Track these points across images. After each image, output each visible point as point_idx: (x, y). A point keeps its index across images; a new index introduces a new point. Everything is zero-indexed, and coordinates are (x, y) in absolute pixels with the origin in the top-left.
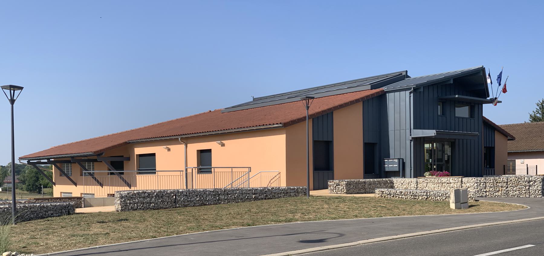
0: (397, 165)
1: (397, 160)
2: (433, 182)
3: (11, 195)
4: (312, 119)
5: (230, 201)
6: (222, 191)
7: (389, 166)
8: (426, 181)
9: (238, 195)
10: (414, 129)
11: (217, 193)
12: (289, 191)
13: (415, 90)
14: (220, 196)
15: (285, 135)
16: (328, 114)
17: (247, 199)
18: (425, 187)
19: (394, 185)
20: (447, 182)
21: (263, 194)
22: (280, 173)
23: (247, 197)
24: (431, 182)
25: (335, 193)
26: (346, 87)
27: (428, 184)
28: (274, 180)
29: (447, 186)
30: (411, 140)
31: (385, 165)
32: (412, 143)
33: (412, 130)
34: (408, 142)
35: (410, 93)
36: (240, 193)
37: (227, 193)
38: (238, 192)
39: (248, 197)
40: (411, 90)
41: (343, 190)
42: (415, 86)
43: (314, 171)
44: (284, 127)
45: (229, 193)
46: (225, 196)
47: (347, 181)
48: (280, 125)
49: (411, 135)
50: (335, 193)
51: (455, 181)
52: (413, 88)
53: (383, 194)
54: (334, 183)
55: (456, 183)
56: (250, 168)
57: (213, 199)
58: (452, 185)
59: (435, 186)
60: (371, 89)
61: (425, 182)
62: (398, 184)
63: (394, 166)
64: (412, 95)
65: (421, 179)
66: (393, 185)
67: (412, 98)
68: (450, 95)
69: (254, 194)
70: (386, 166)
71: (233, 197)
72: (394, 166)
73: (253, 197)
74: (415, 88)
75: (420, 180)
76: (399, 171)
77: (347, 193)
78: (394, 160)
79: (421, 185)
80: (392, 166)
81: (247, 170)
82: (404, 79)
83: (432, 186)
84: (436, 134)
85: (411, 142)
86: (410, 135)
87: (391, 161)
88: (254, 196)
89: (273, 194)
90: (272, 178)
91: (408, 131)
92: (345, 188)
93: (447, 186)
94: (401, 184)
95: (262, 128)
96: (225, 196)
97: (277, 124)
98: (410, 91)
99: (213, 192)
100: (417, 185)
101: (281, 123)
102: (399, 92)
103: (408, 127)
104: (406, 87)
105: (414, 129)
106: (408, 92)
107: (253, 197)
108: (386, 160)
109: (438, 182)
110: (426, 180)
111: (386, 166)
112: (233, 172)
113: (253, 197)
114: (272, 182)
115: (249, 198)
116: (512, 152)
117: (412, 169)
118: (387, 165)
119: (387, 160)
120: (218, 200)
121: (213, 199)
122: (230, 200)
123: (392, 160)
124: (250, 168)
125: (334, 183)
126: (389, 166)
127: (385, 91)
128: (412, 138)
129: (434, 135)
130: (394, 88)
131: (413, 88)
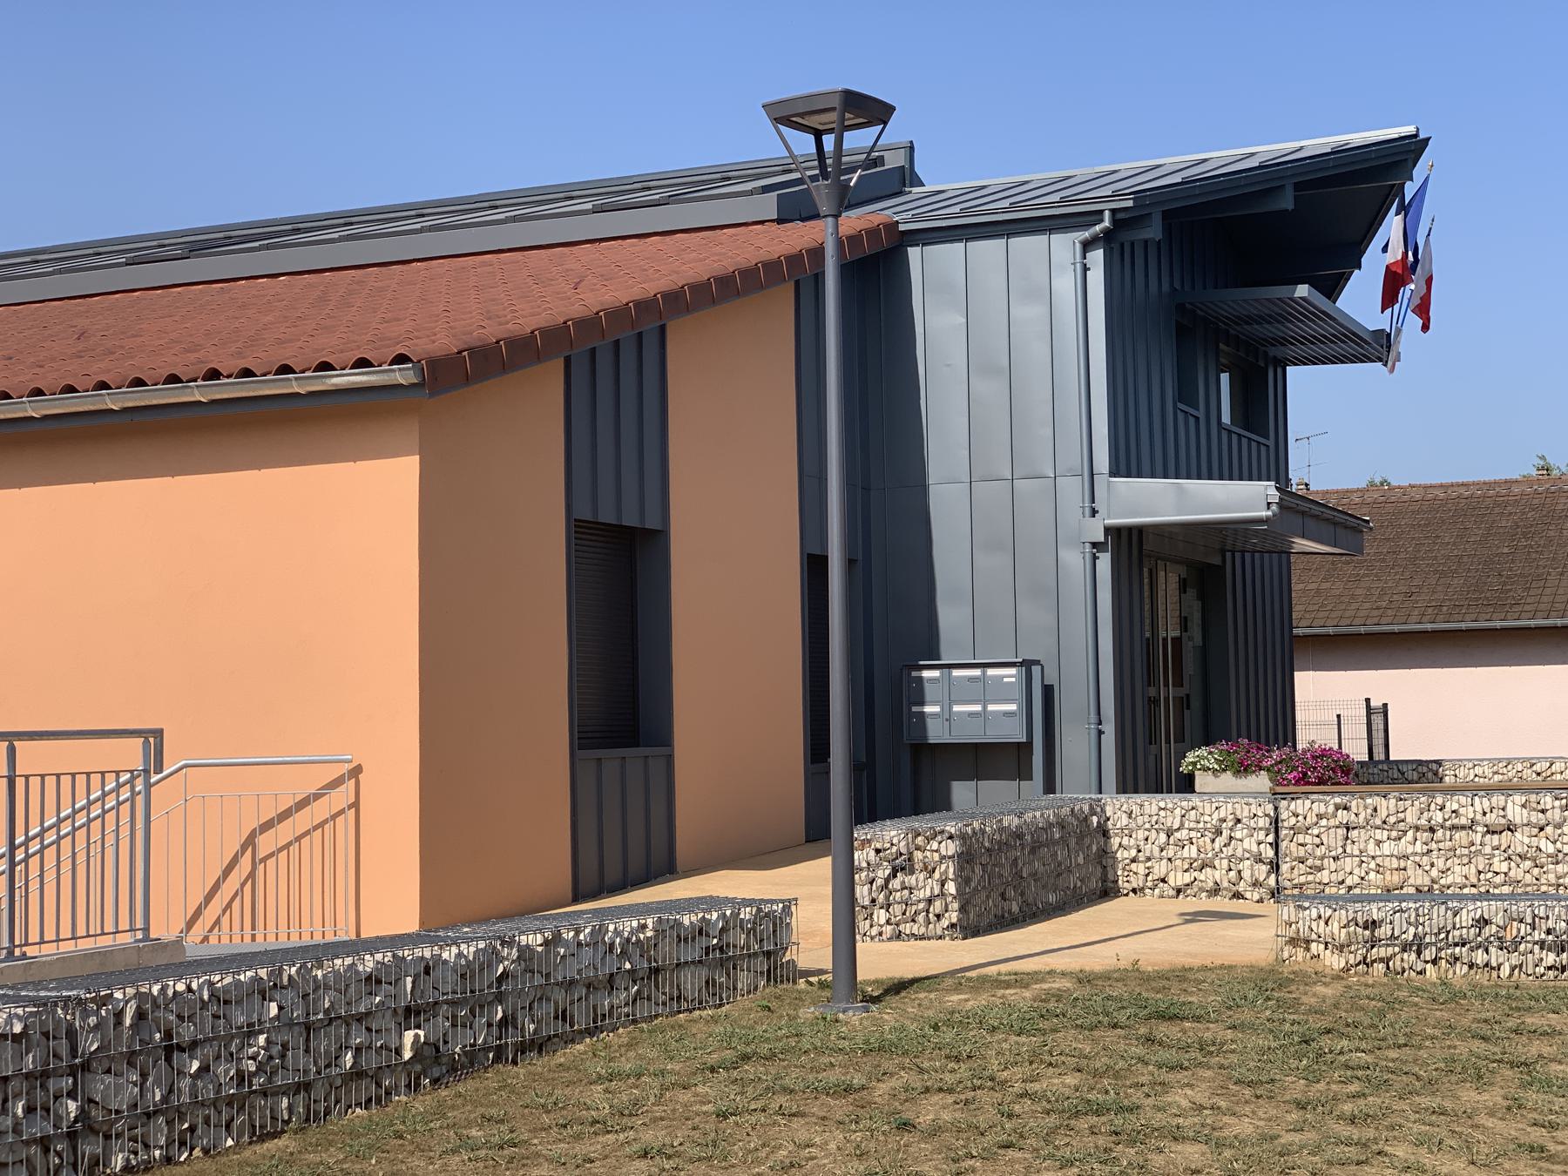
0: (1013, 707)
1: (1013, 671)
2: (1392, 819)
3: (408, 369)
4: (559, 363)
5: (192, 1129)
6: (119, 1015)
7: (956, 708)
8: (1343, 816)
9: (276, 1050)
10: (1114, 472)
11: (63, 1048)
12: (668, 952)
13: (1122, 221)
14: (100, 1085)
15: (414, 460)
16: (640, 335)
17: (357, 1074)
18: (1335, 859)
19: (1115, 841)
20: (1491, 818)
21: (479, 1005)
22: (356, 772)
23: (349, 1058)
24: (1378, 822)
25: (888, 930)
26: (589, 206)
27: (1354, 834)
28: (285, 832)
29: (1488, 850)
30: (1094, 545)
31: (922, 703)
32: (1105, 562)
33: (1102, 481)
34: (1074, 560)
35: (1087, 246)
36: (291, 1024)
37: (168, 1035)
38: (273, 1009)
39: (358, 1050)
40: (1098, 228)
41: (937, 906)
42: (1130, 204)
43: (578, 752)
44: (432, 395)
45: (187, 1032)
46: (144, 1076)
47: (963, 837)
48: (402, 375)
49: (1094, 512)
50: (888, 930)
51: (1543, 811)
52: (1113, 211)
53: (1373, 943)
54: (878, 851)
55: (1549, 829)
56: (158, 734)
57: (16, 1130)
58: (1521, 841)
59: (1404, 845)
60: (780, 221)
61: (1332, 822)
62: (1141, 834)
63: (991, 708)
64: (1097, 257)
65: (1308, 803)
66: (1106, 843)
67: (1097, 277)
68: (1216, 288)
69: (411, 1015)
70: (928, 709)
71: (225, 1071)
72: (991, 708)
73: (398, 1051)
74: (1120, 216)
75: (1300, 806)
76: (1028, 745)
77: (969, 929)
78: (991, 672)
79: (1308, 839)
80: (978, 708)
81: (131, 754)
82: (900, 193)
83: (1387, 848)
84: (1274, 507)
85: (1095, 558)
86: (1087, 511)
87: (971, 679)
88: (409, 1036)
89: (559, 995)
90: (273, 814)
91: (1072, 490)
92: (951, 888)
93: (1488, 850)
94: (1163, 837)
95: (296, 389)
96: (144, 1076)
97: (362, 363)
98: (1086, 234)
99: (16, 1038)
100: (1276, 845)
101: (401, 359)
102: (960, 240)
103: (1073, 455)
104: (1005, 211)
105: (1114, 472)
106: (1065, 245)
107: (407, 1055)
108: (926, 674)
109: (1423, 822)
110: (1337, 807)
111: (928, 709)
112: (20, 782)
113: (407, 1055)
114: (266, 843)
115: (371, 1062)
116: (1556, 628)
117: (1109, 729)
118: (934, 703)
119: (936, 673)
120: (72, 1136)
121: (16, 1130)
122: (201, 1113)
123: (977, 672)
124: (158, 734)
125: (878, 851)
126: (956, 708)
127: (902, 228)
128: (1108, 530)
129: (1265, 513)
130: (964, 213)
131: (1113, 211)
